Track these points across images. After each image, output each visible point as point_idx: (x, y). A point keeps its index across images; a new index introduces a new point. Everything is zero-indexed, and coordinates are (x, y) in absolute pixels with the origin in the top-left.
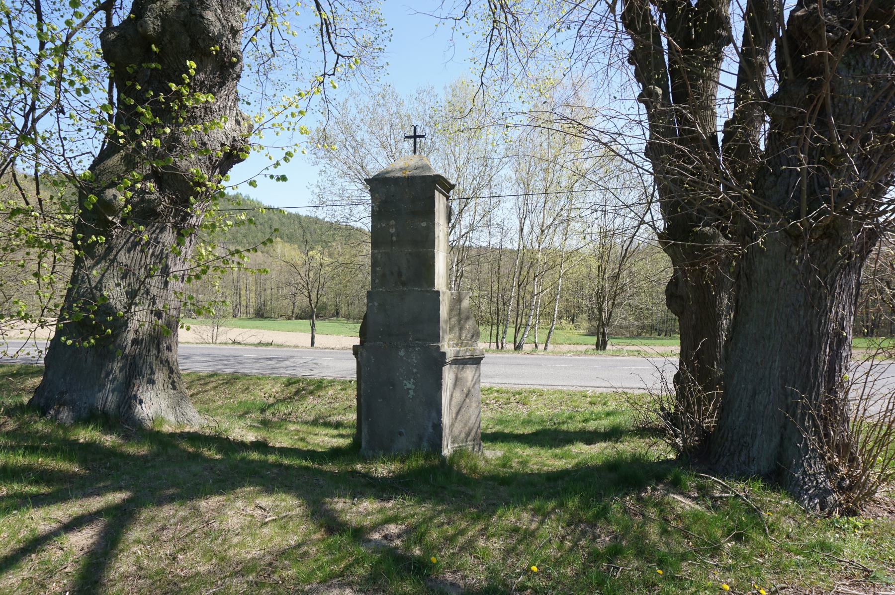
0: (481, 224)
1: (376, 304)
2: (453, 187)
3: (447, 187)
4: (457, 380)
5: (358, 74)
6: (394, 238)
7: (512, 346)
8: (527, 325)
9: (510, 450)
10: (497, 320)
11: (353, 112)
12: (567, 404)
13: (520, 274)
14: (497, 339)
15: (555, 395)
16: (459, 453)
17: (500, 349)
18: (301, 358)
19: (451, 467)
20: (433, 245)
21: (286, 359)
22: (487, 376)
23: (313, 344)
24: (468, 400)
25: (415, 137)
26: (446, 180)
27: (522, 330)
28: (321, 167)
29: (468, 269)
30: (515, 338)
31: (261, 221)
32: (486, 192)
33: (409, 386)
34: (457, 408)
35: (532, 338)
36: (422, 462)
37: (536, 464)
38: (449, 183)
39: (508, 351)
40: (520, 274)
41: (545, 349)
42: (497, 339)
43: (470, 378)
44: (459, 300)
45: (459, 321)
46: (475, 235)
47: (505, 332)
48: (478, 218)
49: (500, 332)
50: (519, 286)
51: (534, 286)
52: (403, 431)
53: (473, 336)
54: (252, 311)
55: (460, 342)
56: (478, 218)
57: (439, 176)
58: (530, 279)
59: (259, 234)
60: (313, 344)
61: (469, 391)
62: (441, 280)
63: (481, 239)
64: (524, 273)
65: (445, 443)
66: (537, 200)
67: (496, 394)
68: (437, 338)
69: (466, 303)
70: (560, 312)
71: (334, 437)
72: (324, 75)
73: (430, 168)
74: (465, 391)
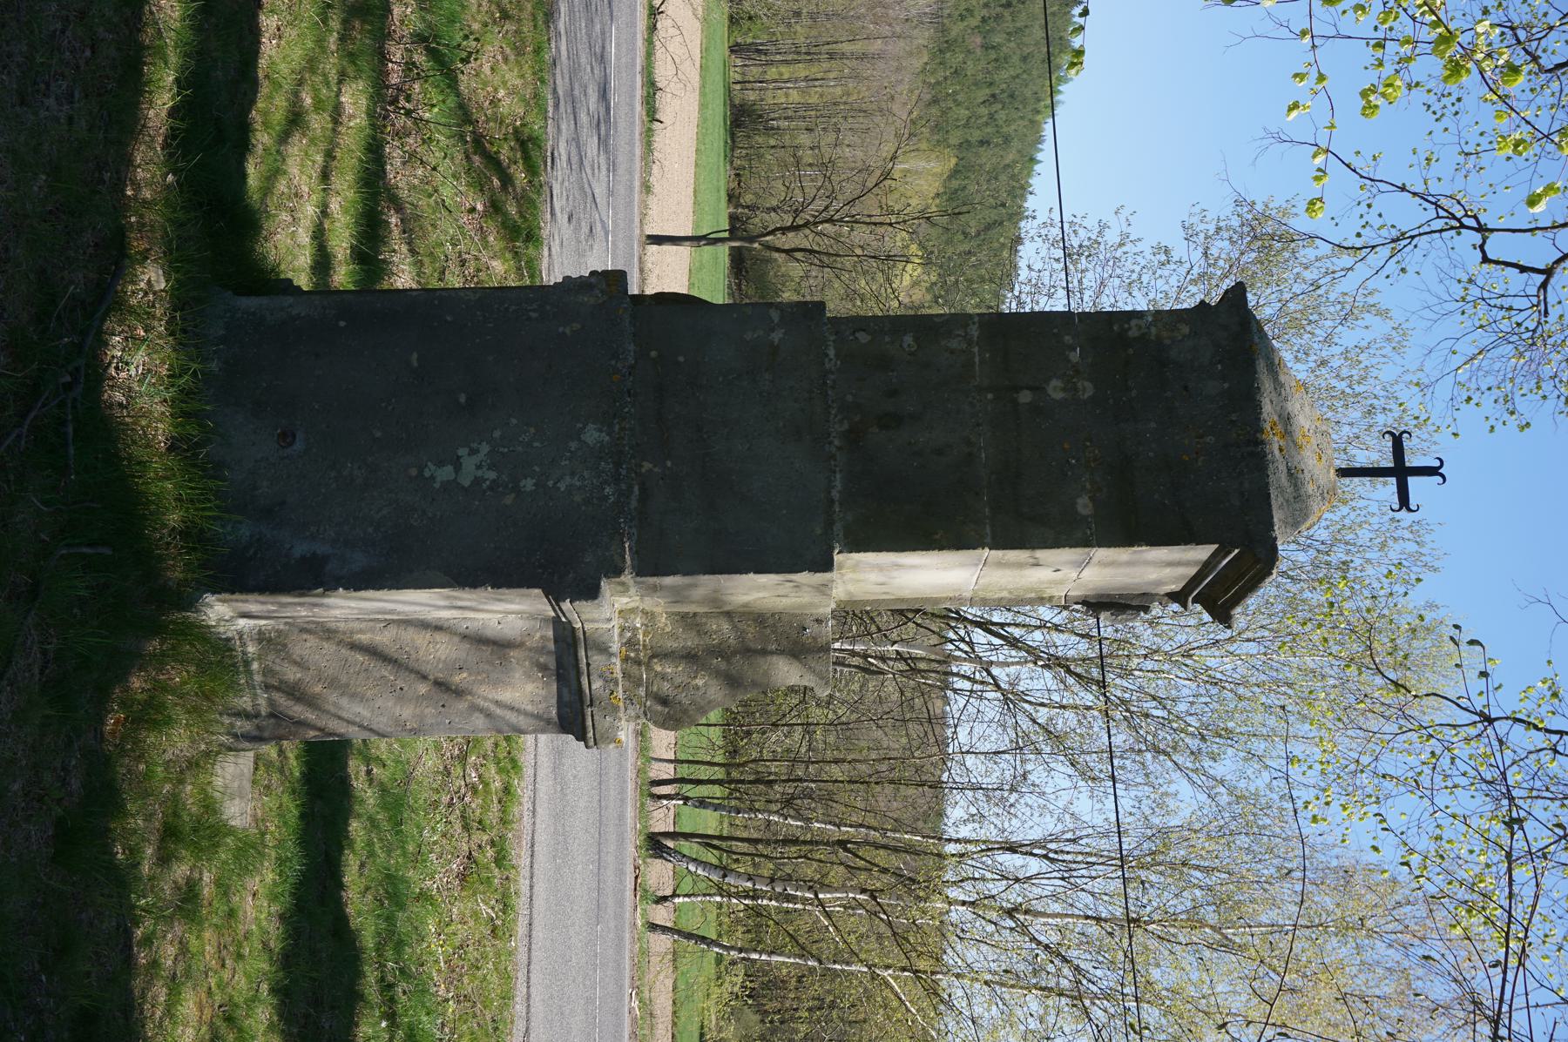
0: (1025, 724)
1: (776, 336)
2: (1223, 616)
3: (1218, 595)
4: (495, 647)
5: (1484, 338)
6: (1025, 397)
7: (659, 827)
8: (725, 871)
9: (248, 850)
10: (741, 780)
11: (1349, 337)
12: (463, 1019)
13: (877, 846)
14: (682, 781)
15: (494, 979)
16: (219, 658)
17: (651, 790)
18: (610, 193)
19: (158, 630)
20: (1005, 540)
21: (603, 142)
22: (558, 753)
23: (658, 240)
24: (423, 688)
25: (1401, 472)
26: (1253, 585)
27: (711, 857)
28: (1180, 250)
29: (890, 687)
30: (687, 836)
31: (1002, 115)
32: (1121, 739)
33: (469, 464)
34: (392, 651)
35: (686, 886)
36: (174, 518)
37: (184, 949)
38: (1238, 599)
39: (643, 813)
40: (877, 846)
41: (653, 927)
42: (682, 781)
43: (506, 695)
44: (800, 647)
45: (720, 651)
46: (991, 707)
47: (702, 803)
48: (1042, 715)
49: (703, 791)
50: (842, 844)
51: (843, 888)
52: (298, 446)
53: (664, 701)
54: (752, 96)
55: (640, 657)
56: (1042, 715)
57: (1271, 556)
58: (863, 876)
59: (964, 113)
60: (658, 240)
61: (459, 693)
62: (874, 577)
63: (975, 726)
64: (881, 857)
65: (253, 604)
66: (1102, 891)
67: (497, 785)
68: (652, 565)
69: (787, 673)
70: (766, 969)
71: (319, 235)
72: (1481, 229)
73: (1296, 525)
74: (459, 678)
